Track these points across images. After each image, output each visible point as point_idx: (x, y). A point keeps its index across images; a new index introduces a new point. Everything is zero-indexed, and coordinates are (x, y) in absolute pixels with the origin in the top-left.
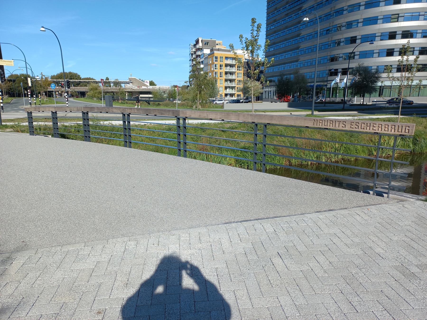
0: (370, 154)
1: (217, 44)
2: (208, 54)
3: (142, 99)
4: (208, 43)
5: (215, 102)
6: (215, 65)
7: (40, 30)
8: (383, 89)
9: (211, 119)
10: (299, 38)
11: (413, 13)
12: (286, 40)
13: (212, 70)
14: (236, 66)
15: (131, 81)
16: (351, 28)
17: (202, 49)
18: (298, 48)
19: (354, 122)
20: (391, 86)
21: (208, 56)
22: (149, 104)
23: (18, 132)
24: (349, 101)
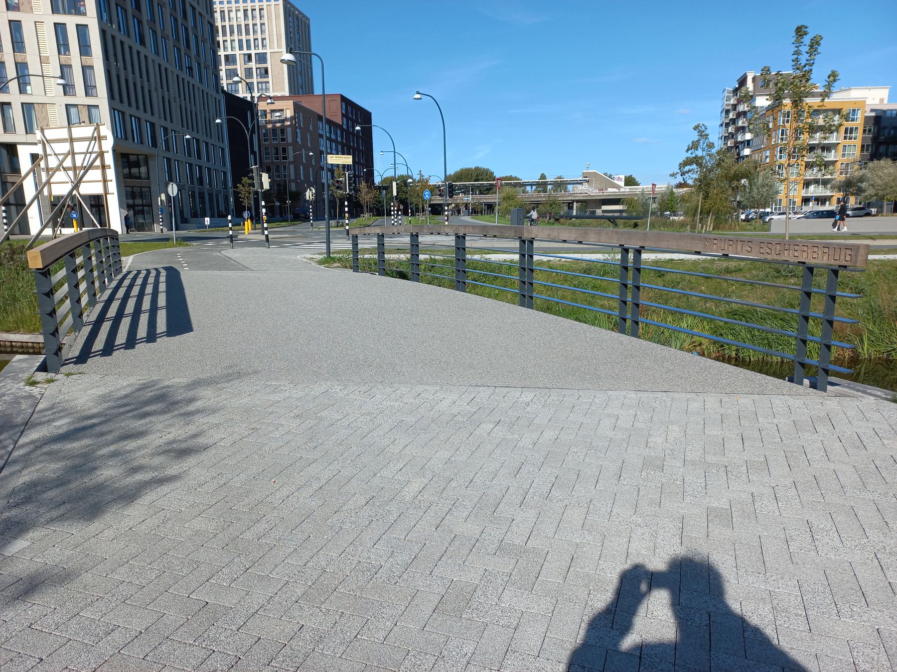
2: (766, 108)
3: (606, 214)
5: (769, 218)
7: (414, 99)
9: (565, 241)
13: (773, 143)
15: (587, 179)
21: (765, 112)
22: (616, 225)
23: (346, 267)
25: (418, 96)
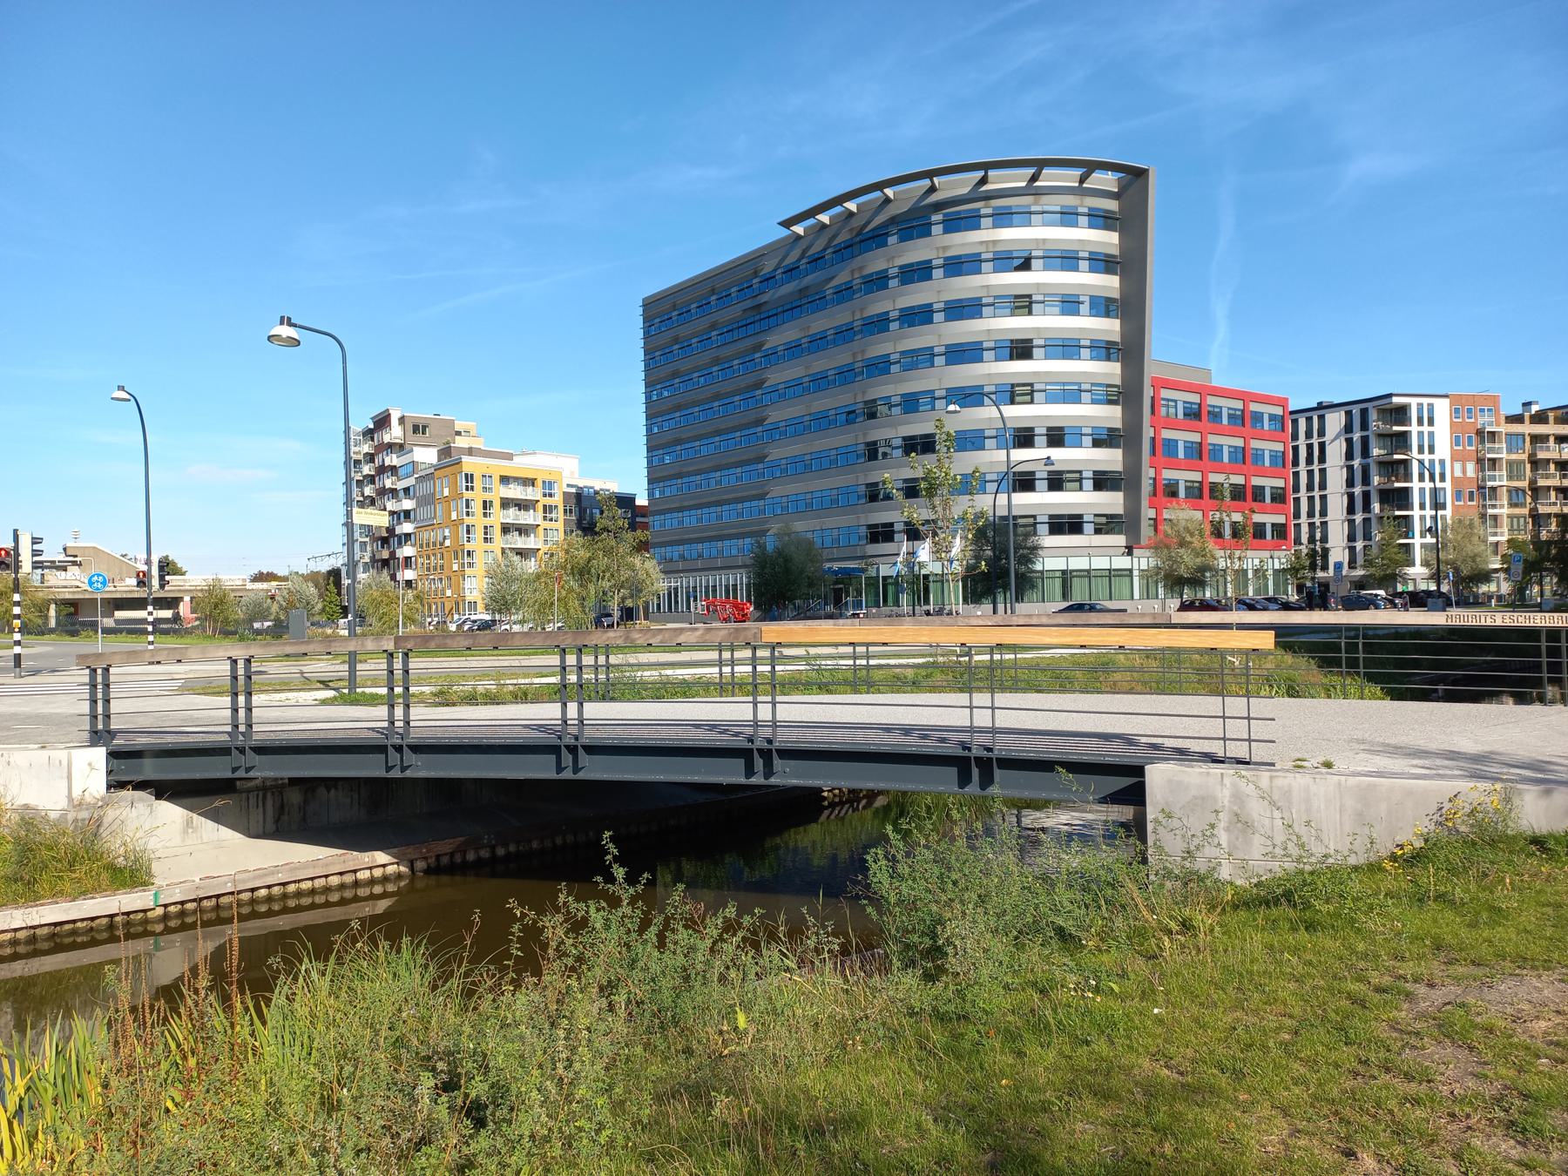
1: (458, 433)
4: (424, 427)
6: (467, 501)
10: (760, 429)
11: (1064, 384)
12: (718, 433)
14: (540, 507)
15: (72, 559)
16: (917, 411)
17: (401, 446)
18: (761, 459)
20: (1088, 571)
21: (432, 470)
25: (286, 331)
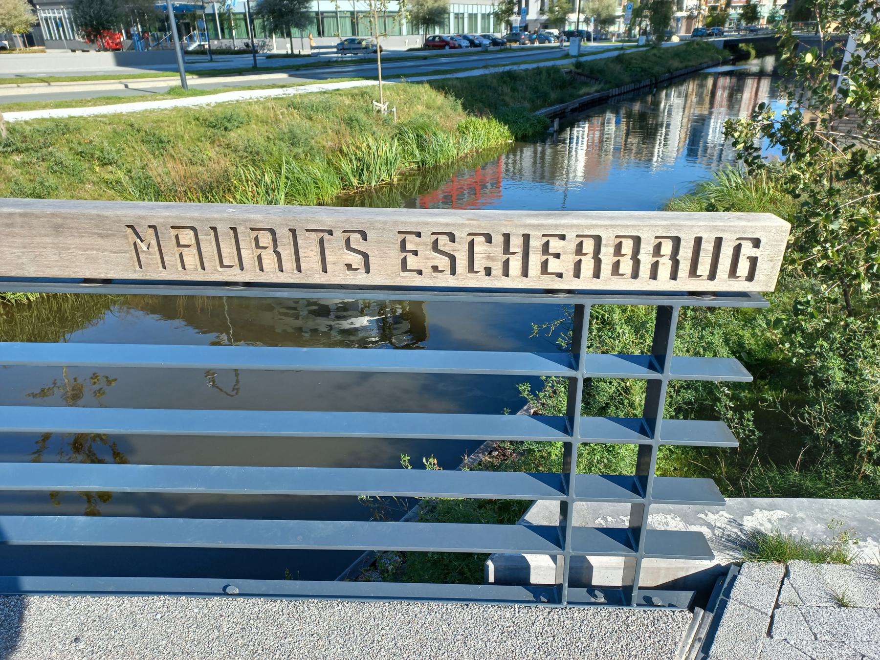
0: (346, 185)
8: (322, 19)
19: (419, 235)
20: (336, 13)
24: (263, 47)
